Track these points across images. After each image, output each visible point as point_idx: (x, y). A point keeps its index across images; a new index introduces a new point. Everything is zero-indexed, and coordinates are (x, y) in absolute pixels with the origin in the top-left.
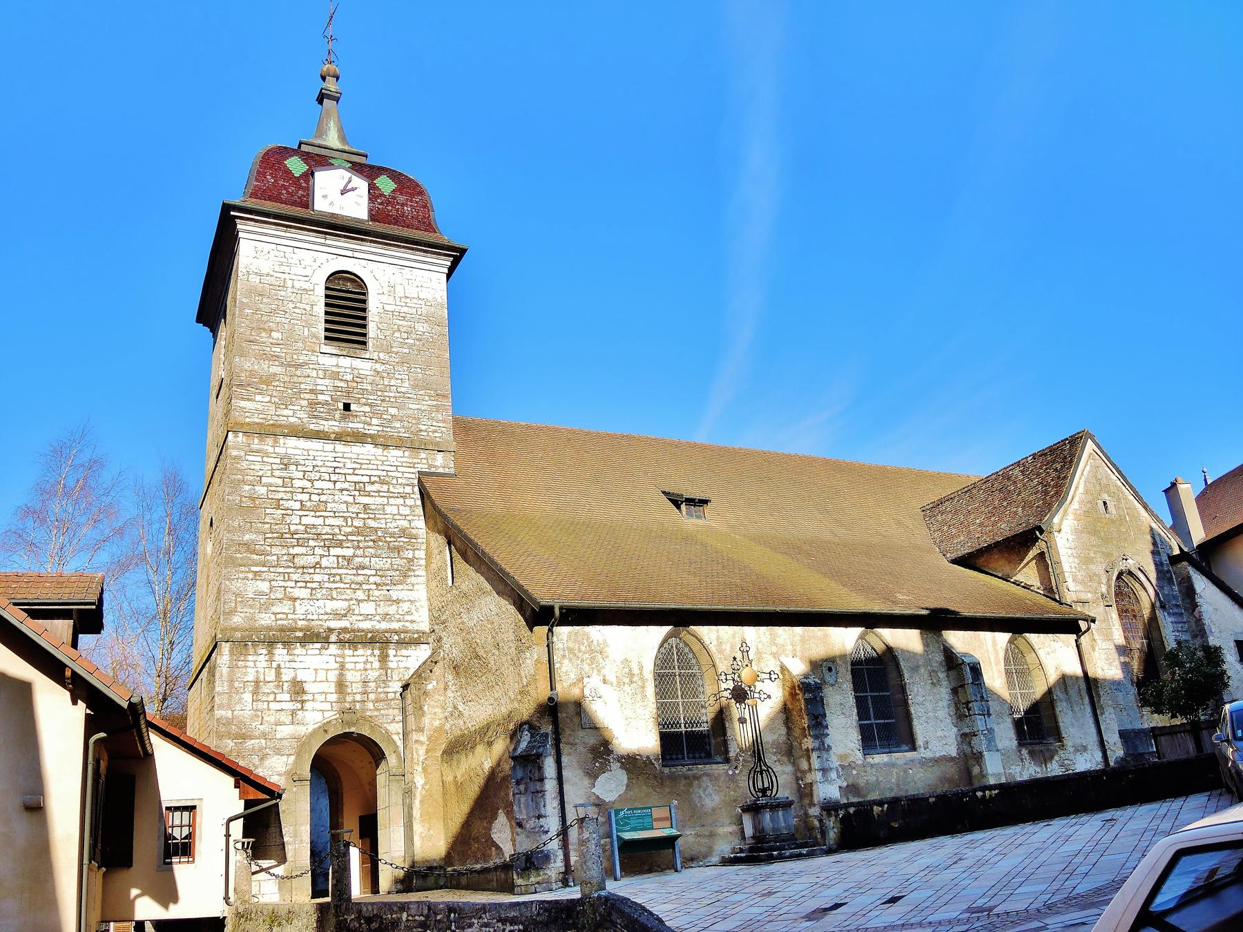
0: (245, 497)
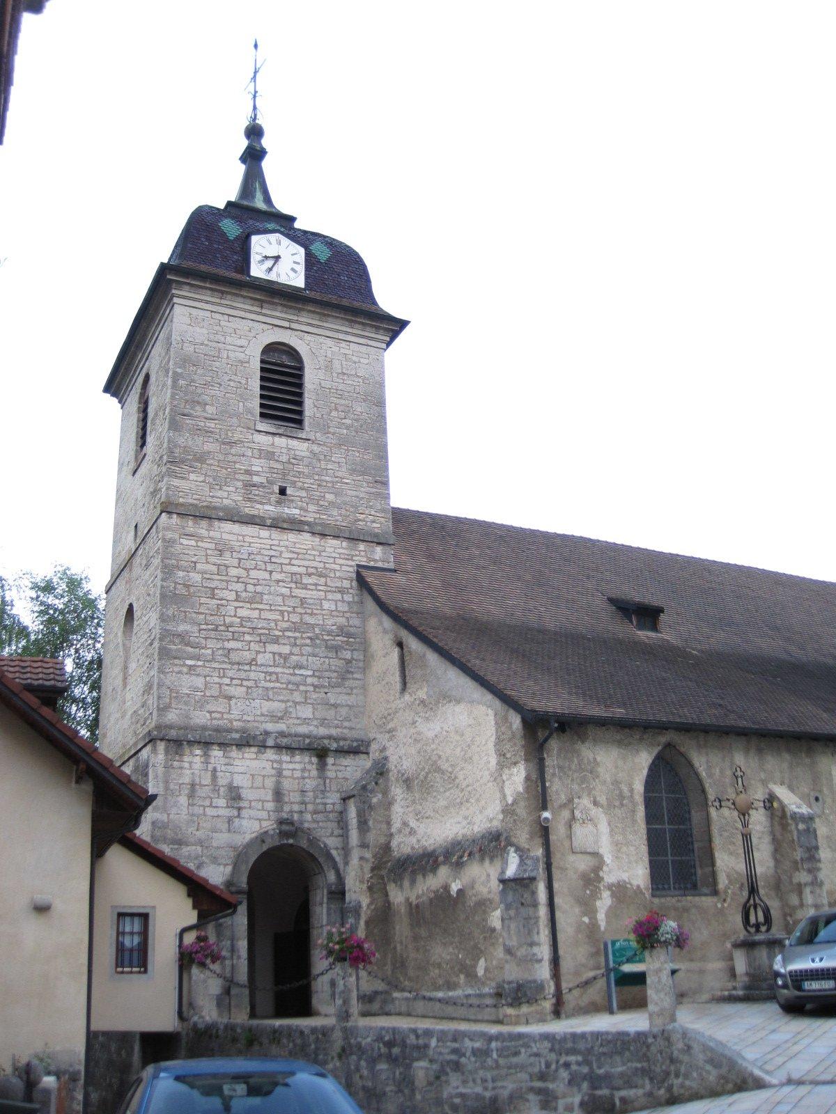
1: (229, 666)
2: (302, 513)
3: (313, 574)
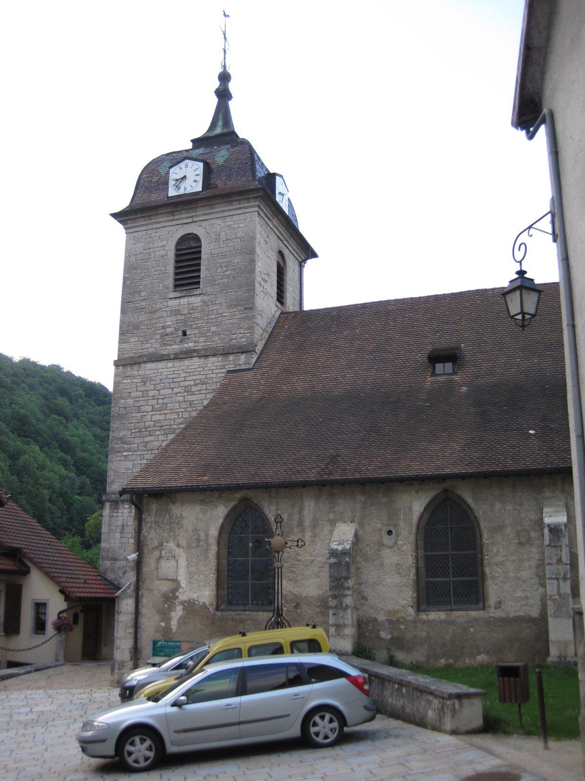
0: (121, 407)
2: (196, 345)
3: (199, 384)
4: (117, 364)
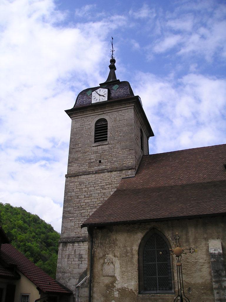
1: (81, 218)
2: (106, 166)
4: (67, 176)
